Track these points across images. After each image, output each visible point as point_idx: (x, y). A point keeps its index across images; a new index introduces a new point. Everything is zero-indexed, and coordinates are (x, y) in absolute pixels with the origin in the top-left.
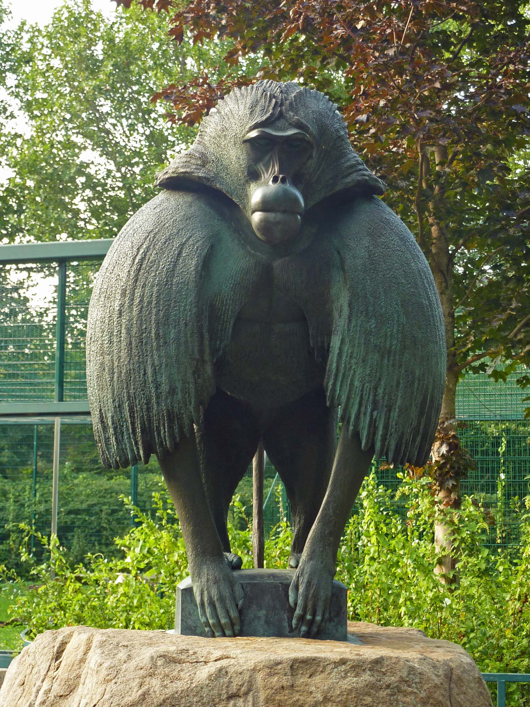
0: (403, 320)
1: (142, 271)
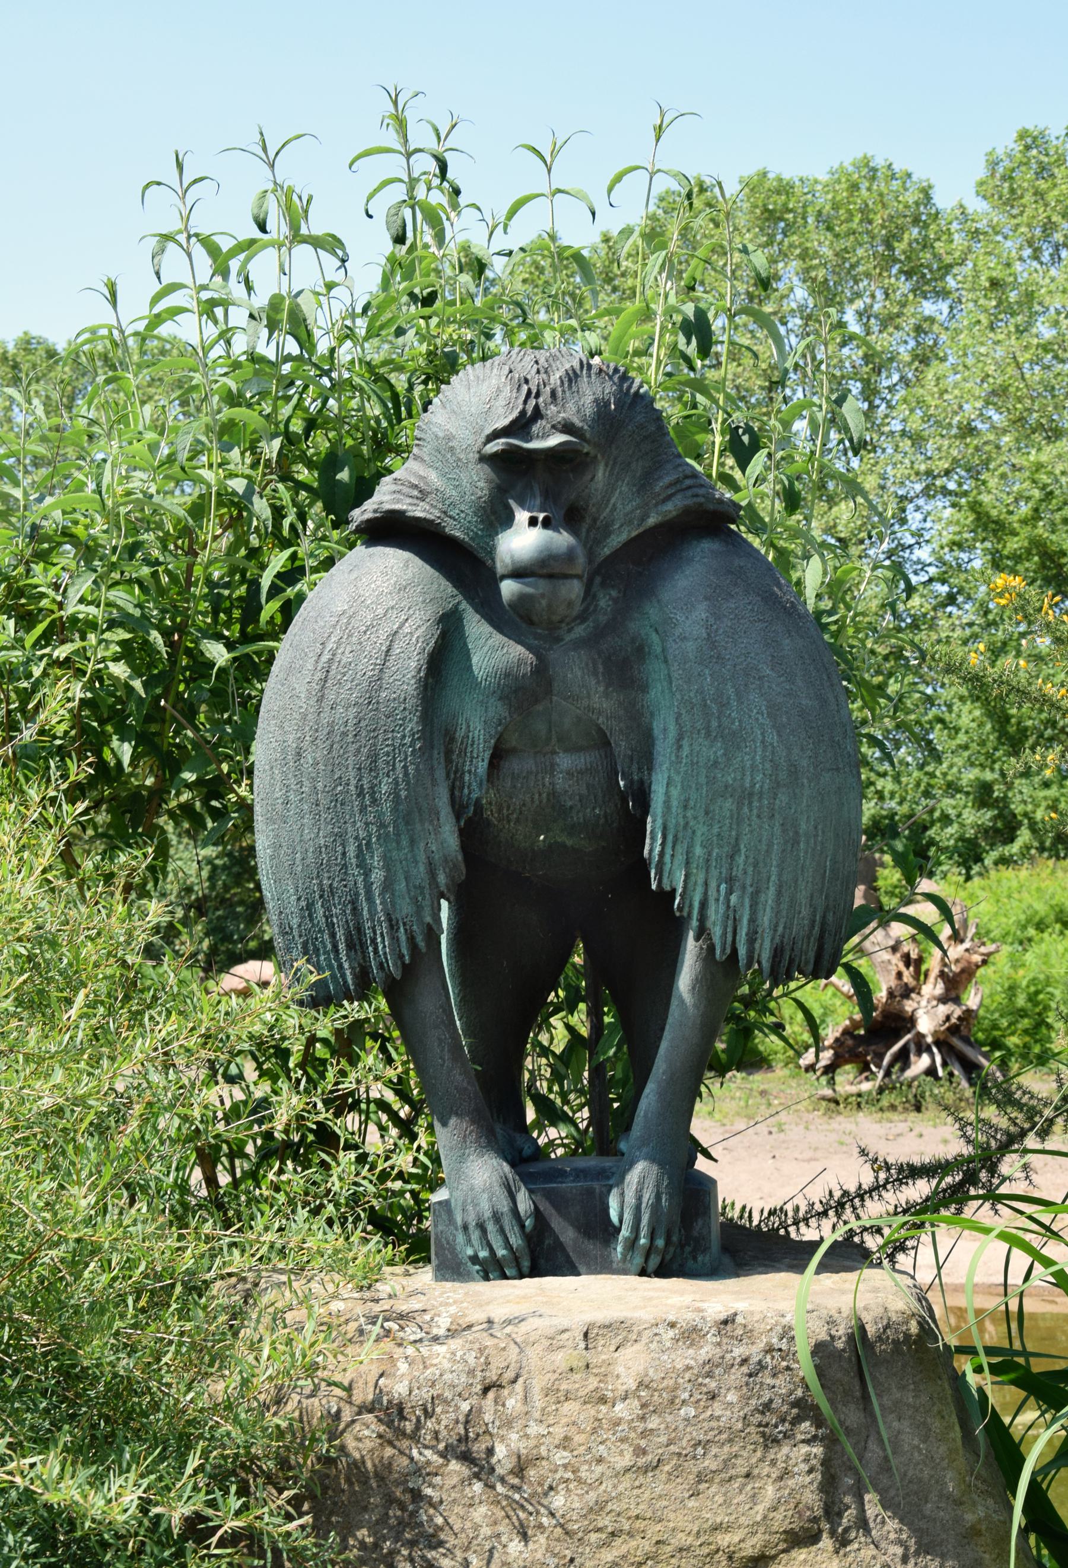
0: (772, 737)
1: (330, 682)
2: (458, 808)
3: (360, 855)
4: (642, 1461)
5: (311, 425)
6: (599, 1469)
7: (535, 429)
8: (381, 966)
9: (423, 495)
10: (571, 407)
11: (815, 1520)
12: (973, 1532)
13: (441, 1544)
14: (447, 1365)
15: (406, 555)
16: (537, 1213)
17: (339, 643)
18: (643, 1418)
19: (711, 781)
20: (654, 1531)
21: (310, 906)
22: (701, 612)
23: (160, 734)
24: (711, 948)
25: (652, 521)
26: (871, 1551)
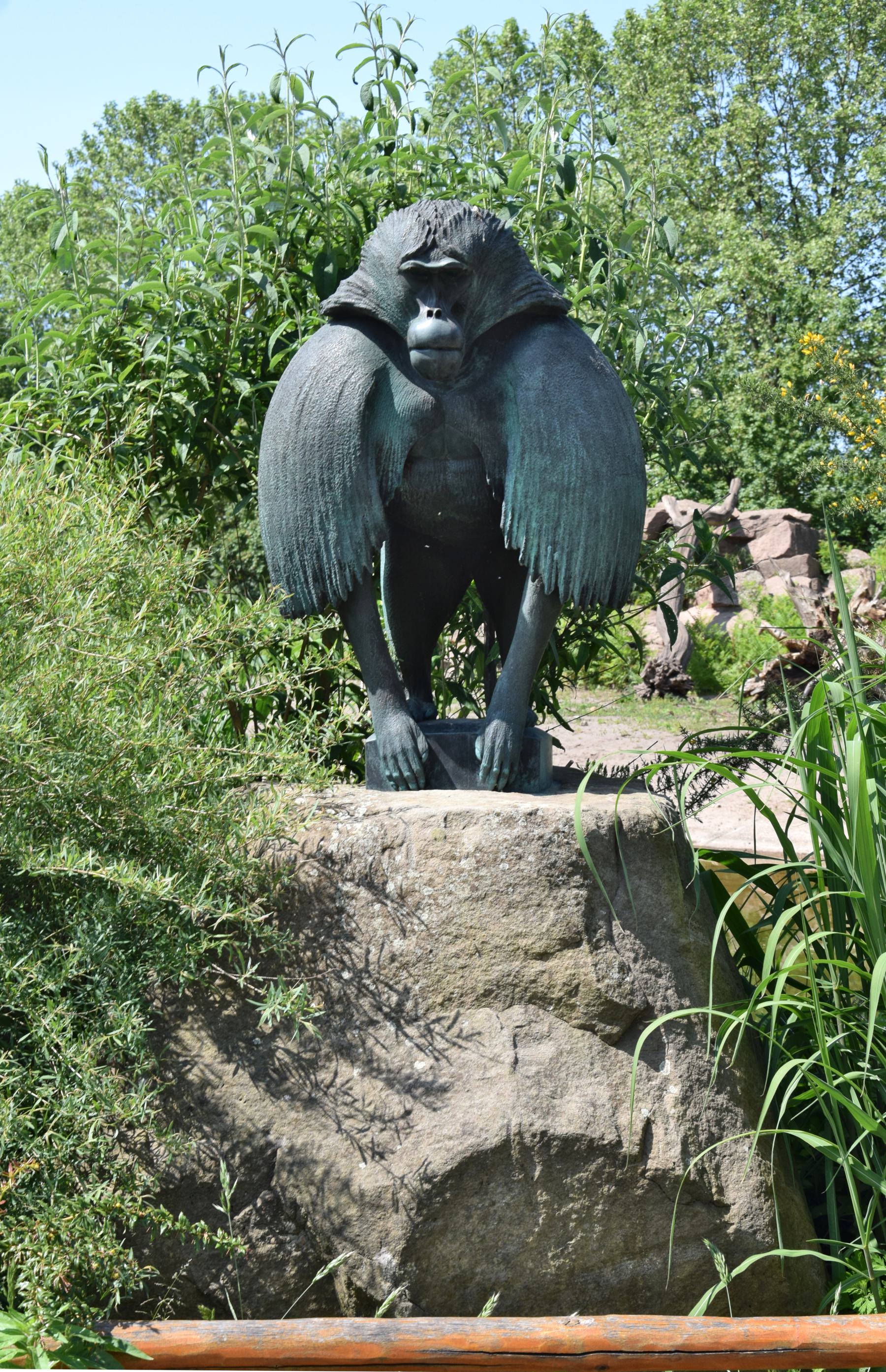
0: (583, 453)
2: (384, 494)
3: (321, 522)
4: (475, 894)
5: (310, 233)
6: (450, 898)
7: (432, 254)
8: (334, 593)
9: (365, 293)
10: (456, 240)
11: (579, 933)
12: (685, 949)
13: (354, 939)
14: (361, 834)
15: (354, 331)
16: (430, 750)
17: (310, 387)
18: (477, 869)
19: (543, 480)
20: (481, 935)
21: (291, 554)
22: (539, 372)
23: (209, 440)
24: (542, 587)
25: (510, 313)
26: (614, 953)
